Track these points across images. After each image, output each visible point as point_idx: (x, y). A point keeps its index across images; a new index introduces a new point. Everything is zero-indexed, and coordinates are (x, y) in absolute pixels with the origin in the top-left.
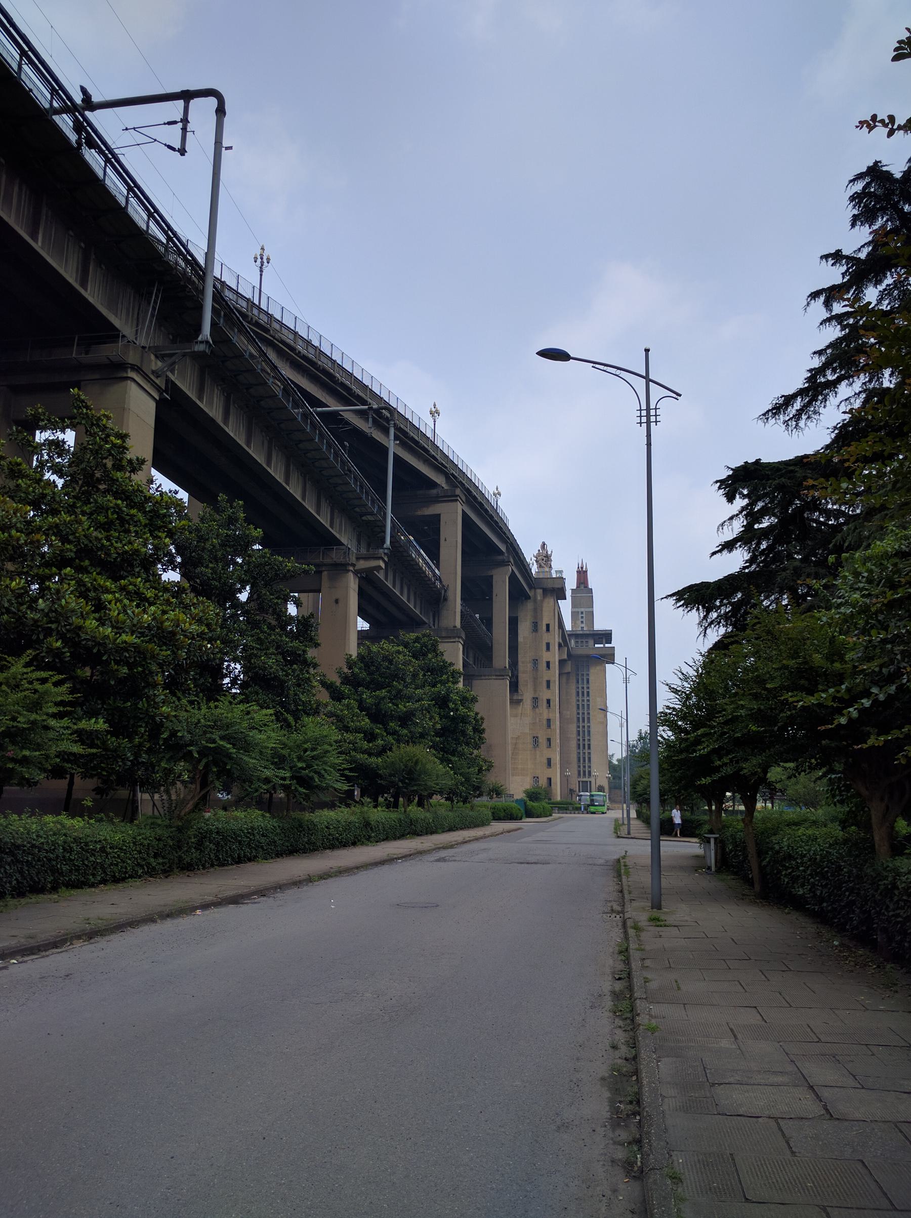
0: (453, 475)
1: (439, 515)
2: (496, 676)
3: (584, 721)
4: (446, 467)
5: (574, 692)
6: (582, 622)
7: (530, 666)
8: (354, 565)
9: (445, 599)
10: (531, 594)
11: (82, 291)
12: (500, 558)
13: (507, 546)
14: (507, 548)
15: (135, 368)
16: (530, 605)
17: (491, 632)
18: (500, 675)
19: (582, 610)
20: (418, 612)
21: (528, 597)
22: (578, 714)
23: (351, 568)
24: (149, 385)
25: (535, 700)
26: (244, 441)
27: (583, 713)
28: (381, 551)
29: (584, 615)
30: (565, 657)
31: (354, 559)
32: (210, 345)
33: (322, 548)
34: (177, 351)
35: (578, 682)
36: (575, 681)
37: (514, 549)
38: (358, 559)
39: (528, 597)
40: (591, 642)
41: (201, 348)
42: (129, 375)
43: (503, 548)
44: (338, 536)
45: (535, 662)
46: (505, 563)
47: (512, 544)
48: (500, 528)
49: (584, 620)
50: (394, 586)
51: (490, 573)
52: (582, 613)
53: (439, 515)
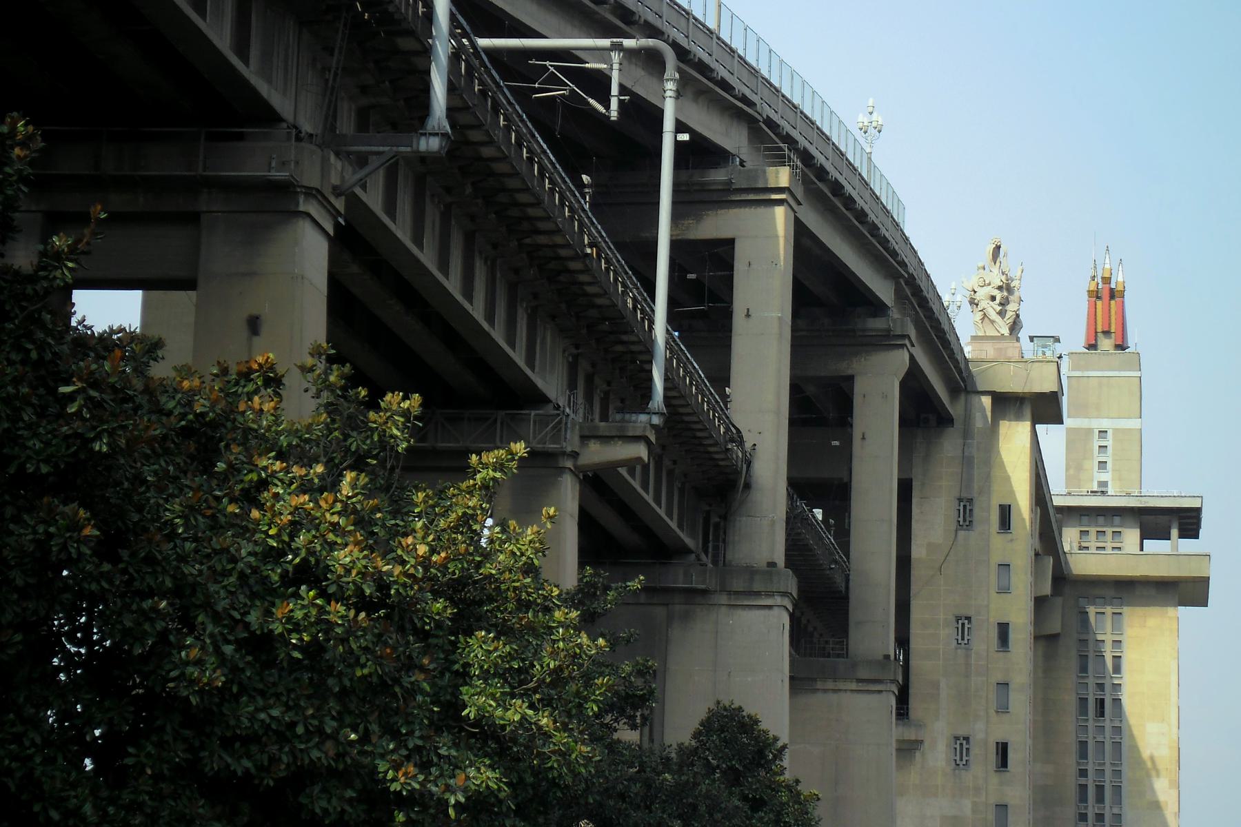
0: (770, 123)
1: (730, 243)
2: (859, 681)
3: (1100, 798)
4: (751, 104)
5: (1071, 701)
6: (1102, 464)
7: (947, 633)
8: (575, 455)
9: (748, 486)
10: (956, 410)
11: (467, 305)
12: (877, 324)
13: (898, 285)
14: (899, 293)
15: (311, 193)
16: (949, 445)
17: (845, 547)
18: (869, 684)
19: (1105, 424)
20: (673, 525)
21: (945, 420)
22: (1083, 773)
23: (569, 464)
24: (323, 212)
25: (962, 744)
26: (409, 234)
27: (1101, 772)
28: (643, 418)
29: (1109, 442)
30: (1047, 589)
31: (576, 439)
32: (449, 137)
33: (502, 413)
34: (381, 149)
35: (1084, 669)
36: (1074, 663)
37: (917, 291)
38: (584, 438)
39: (945, 420)
40: (1131, 536)
41: (434, 144)
42: (302, 208)
43: (883, 290)
44: (263, 88)
45: (963, 622)
46: (888, 341)
47: (911, 281)
48: (884, 242)
49: (1108, 457)
50: (418, 240)
51: (843, 368)
52: (1103, 433)
53: (730, 243)
